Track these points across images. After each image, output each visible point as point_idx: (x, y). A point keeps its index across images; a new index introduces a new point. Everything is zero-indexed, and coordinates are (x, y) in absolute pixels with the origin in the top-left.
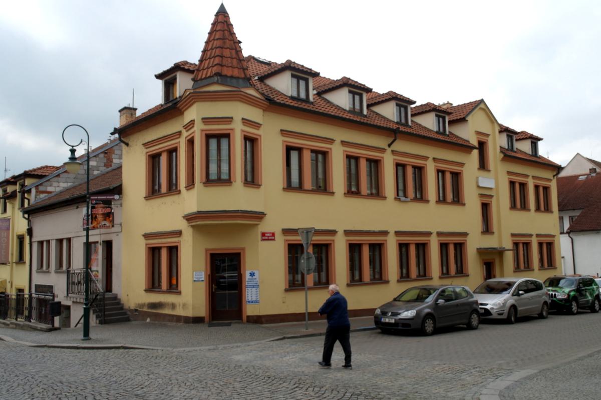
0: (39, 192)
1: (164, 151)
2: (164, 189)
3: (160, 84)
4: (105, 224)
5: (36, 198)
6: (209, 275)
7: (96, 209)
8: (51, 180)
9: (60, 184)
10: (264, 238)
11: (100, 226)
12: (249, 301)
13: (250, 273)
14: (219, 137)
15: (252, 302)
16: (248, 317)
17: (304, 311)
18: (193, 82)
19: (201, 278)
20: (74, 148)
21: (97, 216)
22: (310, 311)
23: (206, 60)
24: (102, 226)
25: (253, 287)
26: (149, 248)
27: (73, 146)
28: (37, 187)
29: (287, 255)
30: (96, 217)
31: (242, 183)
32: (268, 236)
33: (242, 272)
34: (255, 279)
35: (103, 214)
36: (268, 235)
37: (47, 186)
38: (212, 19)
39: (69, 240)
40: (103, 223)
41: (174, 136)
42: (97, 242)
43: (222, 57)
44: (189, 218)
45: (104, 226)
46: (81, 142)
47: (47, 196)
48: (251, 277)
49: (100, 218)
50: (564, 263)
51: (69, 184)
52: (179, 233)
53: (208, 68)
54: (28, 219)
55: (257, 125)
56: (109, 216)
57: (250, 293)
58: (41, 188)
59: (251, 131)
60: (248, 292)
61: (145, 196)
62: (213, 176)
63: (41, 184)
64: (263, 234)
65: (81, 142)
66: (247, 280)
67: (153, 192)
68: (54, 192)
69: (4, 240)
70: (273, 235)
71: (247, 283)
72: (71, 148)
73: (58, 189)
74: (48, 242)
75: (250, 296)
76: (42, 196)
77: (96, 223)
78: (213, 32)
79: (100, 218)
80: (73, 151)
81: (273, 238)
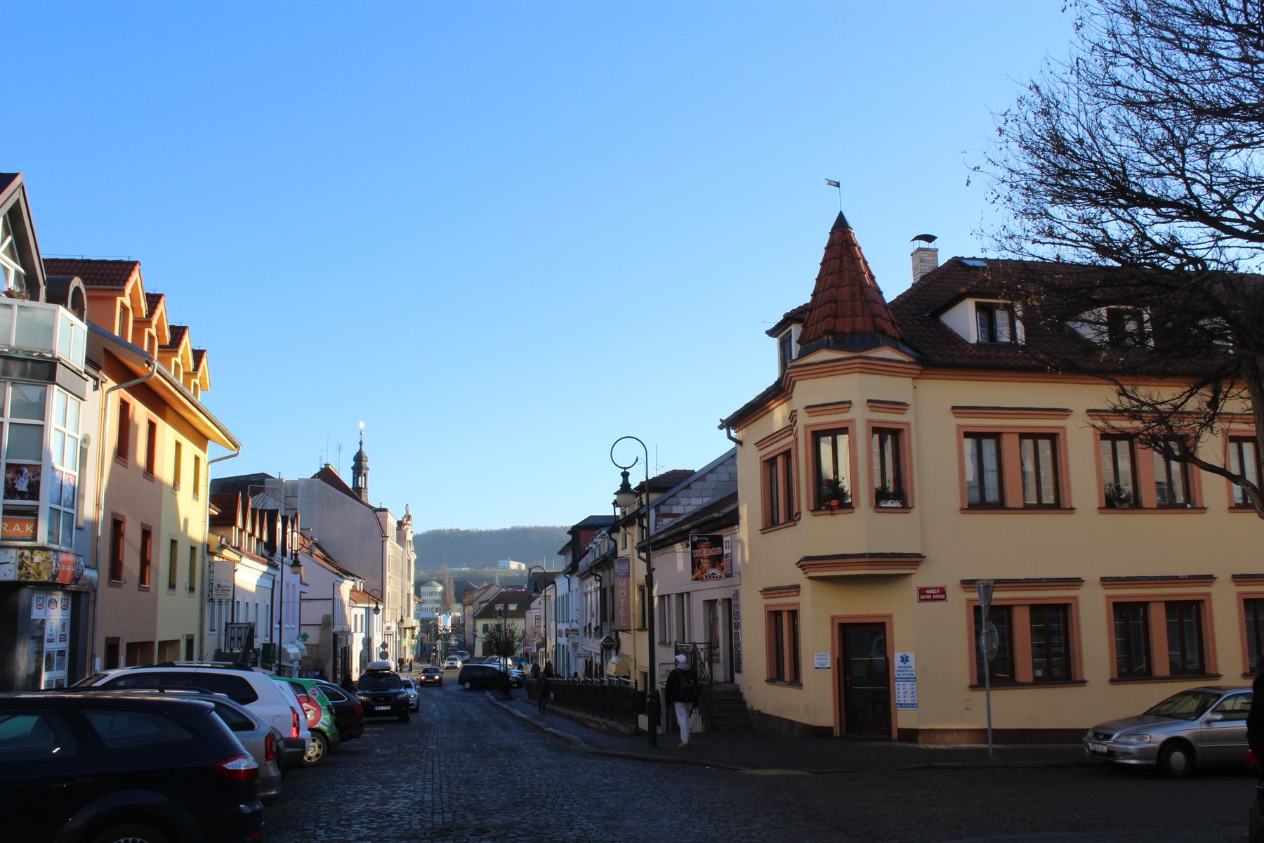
0: (660, 516)
1: (779, 455)
2: (782, 520)
3: (774, 342)
4: (713, 573)
5: (656, 525)
6: (838, 659)
7: (700, 550)
8: (677, 495)
9: (692, 499)
10: (923, 597)
11: (706, 577)
12: (901, 704)
13: (901, 657)
14: (834, 433)
15: (906, 706)
16: (900, 730)
17: (986, 726)
18: (799, 346)
19: (827, 663)
20: (627, 470)
21: (701, 560)
22: (994, 727)
23: (815, 309)
24: (710, 577)
25: (907, 680)
26: (770, 612)
27: (625, 468)
28: (657, 508)
29: (1113, 623)
30: (699, 563)
31: (872, 508)
32: (932, 594)
33: (888, 656)
34: (910, 667)
35: (710, 558)
36: (932, 592)
37: (672, 505)
38: (825, 239)
39: (688, 593)
40: (711, 571)
41: (781, 434)
42: (717, 600)
43: (835, 301)
44: (806, 563)
45: (713, 577)
46: (637, 460)
47: (673, 521)
48: (902, 664)
49: (705, 563)
50: (267, 631)
51: (706, 500)
52: (796, 589)
53: (817, 323)
54: (648, 561)
55: (900, 406)
56: (717, 560)
57: (901, 691)
58: (664, 509)
59: (888, 418)
60: (898, 693)
61: (761, 528)
62: (1045, 445)
63: (663, 503)
64: (922, 591)
65: (637, 460)
66: (896, 668)
67: (771, 523)
68: (682, 514)
69: (622, 594)
70: (942, 591)
71: (896, 673)
72: (623, 470)
73: (689, 510)
74: (669, 595)
75: (901, 695)
76: (666, 521)
77: (699, 572)
78: (827, 261)
79: (705, 563)
80: (625, 475)
81: (942, 596)
